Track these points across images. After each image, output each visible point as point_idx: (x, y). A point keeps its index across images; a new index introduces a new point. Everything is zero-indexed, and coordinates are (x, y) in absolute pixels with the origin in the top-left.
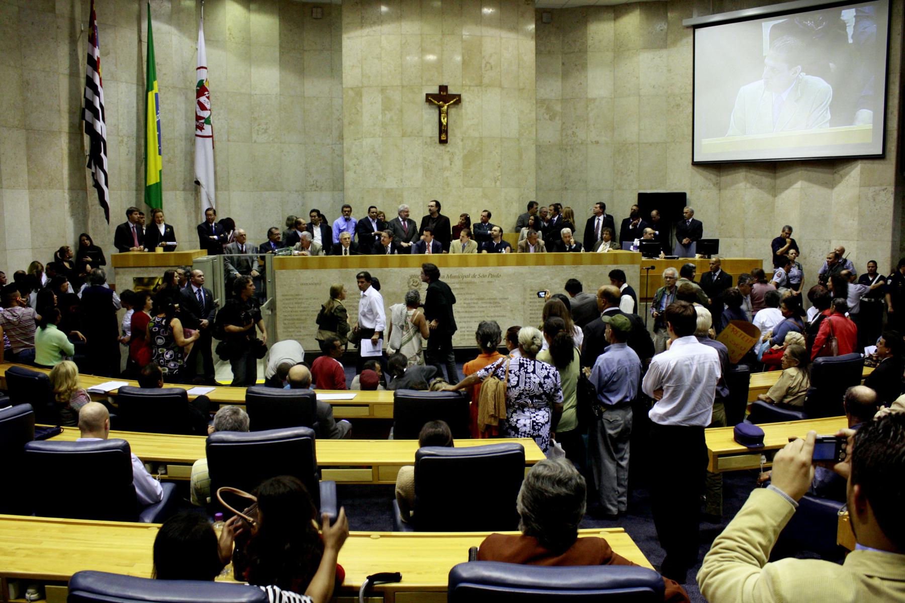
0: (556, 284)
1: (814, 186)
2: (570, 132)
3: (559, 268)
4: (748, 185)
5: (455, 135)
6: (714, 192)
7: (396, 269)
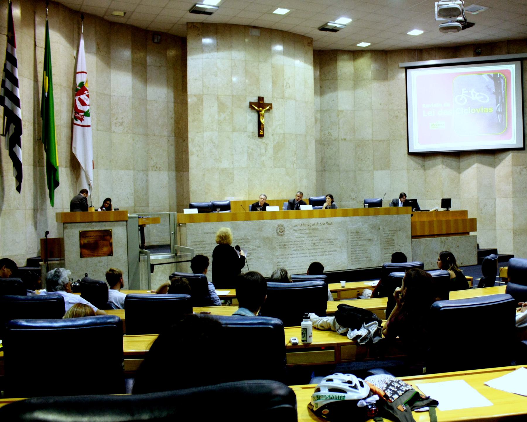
0: (365, 228)
1: (485, 166)
2: (326, 132)
3: (366, 217)
4: (444, 167)
5: (268, 131)
6: (422, 171)
7: (269, 221)
